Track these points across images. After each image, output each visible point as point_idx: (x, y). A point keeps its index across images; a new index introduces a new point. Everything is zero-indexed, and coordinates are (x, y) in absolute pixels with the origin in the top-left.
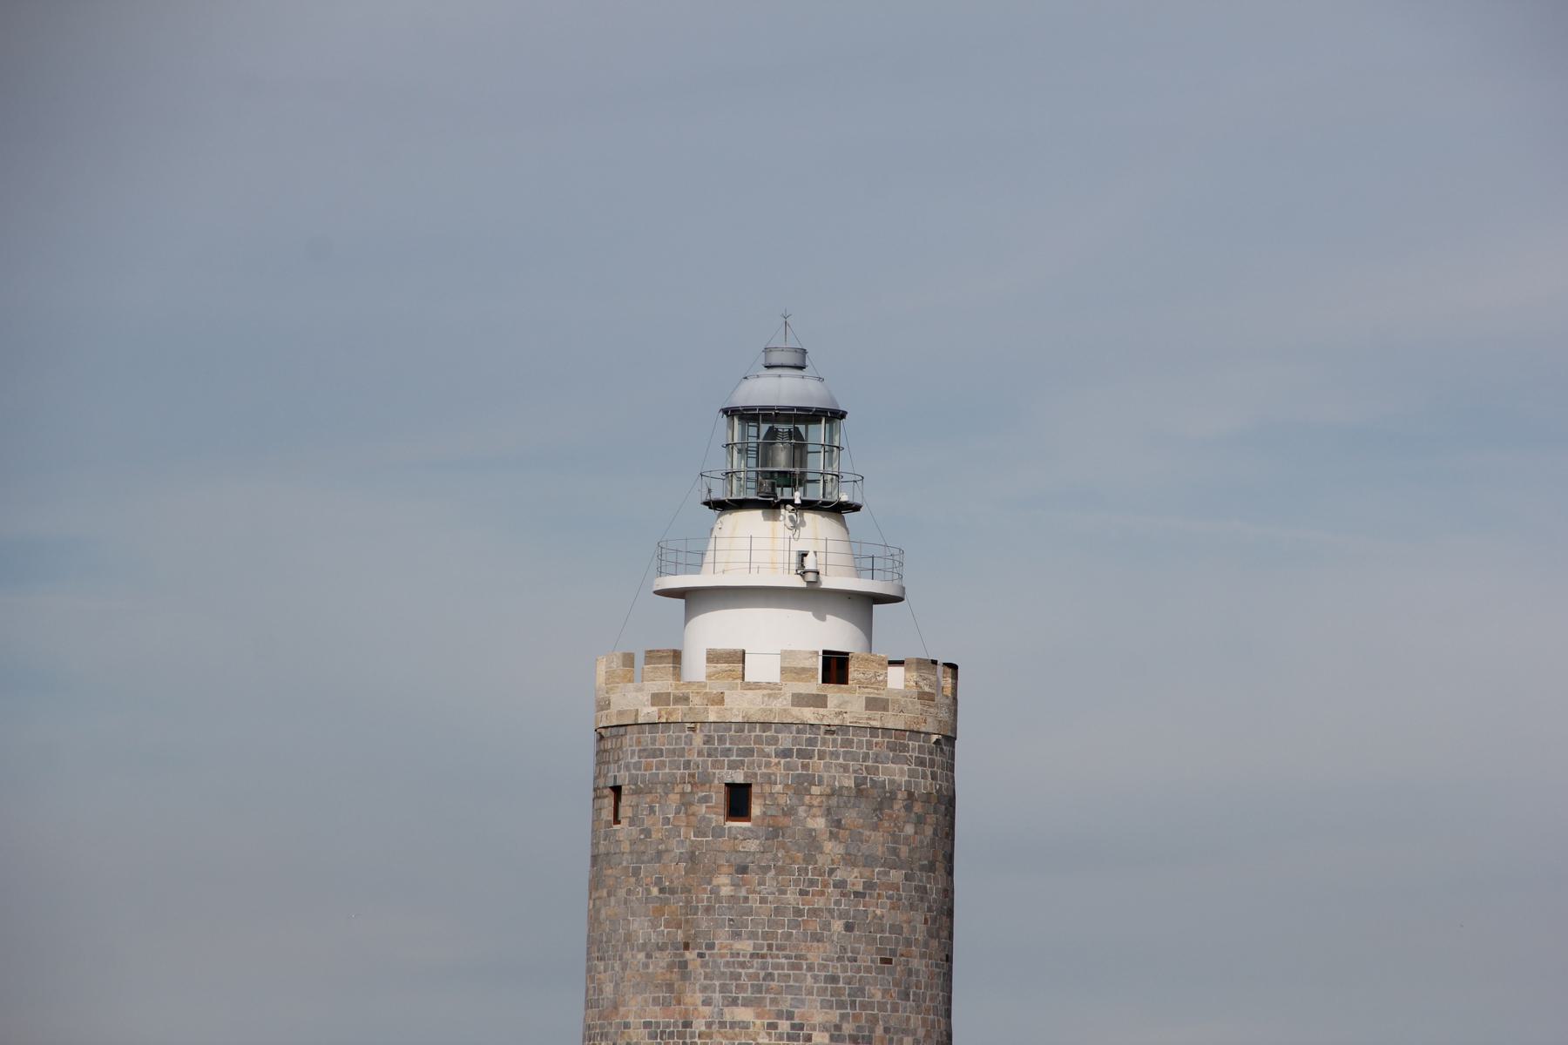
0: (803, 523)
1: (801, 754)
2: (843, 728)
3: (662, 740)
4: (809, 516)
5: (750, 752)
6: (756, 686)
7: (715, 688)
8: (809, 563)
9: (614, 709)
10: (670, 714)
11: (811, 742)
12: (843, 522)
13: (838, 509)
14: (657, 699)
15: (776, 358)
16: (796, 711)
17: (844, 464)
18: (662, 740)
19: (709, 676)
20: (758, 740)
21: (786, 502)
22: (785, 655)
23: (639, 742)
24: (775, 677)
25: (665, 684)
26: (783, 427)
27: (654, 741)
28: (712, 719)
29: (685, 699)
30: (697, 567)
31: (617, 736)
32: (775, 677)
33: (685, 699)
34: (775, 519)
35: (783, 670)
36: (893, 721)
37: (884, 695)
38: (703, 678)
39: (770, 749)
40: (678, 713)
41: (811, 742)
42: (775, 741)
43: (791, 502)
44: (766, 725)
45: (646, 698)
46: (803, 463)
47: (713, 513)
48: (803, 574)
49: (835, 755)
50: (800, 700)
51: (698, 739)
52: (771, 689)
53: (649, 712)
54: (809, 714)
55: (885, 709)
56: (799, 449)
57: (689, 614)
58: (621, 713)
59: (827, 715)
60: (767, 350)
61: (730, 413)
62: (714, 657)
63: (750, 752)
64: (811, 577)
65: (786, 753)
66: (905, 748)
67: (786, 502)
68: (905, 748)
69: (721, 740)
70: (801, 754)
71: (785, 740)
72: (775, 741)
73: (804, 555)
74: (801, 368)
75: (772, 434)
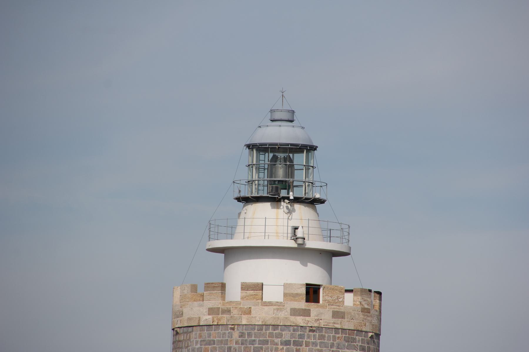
0: (294, 210)
1: (296, 343)
2: (320, 329)
3: (214, 335)
4: (297, 206)
5: (266, 342)
6: (270, 304)
7: (246, 305)
8: (299, 233)
9: (185, 317)
10: (219, 320)
11: (301, 336)
12: (315, 210)
13: (312, 202)
14: (212, 311)
15: (277, 116)
16: (292, 318)
17: (316, 176)
18: (214, 335)
19: (242, 298)
20: (271, 335)
21: (284, 198)
22: (286, 286)
23: (200, 336)
24: (280, 298)
25: (215, 302)
26: (281, 155)
27: (209, 335)
28: (244, 322)
29: (229, 311)
30: (231, 236)
31: (187, 333)
32: (280, 298)
33: (229, 311)
34: (278, 207)
35: (285, 295)
36: (348, 325)
37: (342, 309)
38: (239, 299)
39: (278, 341)
40: (224, 319)
41: (301, 336)
42: (280, 336)
43: (288, 198)
44: (275, 327)
45: (205, 310)
46: (292, 176)
47: (241, 204)
48: (296, 239)
49: (315, 344)
50: (295, 312)
51: (236, 335)
52: (279, 306)
53: (207, 319)
54: (300, 320)
55: (343, 317)
56: (290, 168)
57: (227, 263)
58: (190, 319)
59: (310, 321)
60: (272, 111)
61: (251, 147)
62: (245, 287)
63: (266, 342)
64: (300, 241)
65: (287, 343)
66: (354, 340)
67: (284, 198)
68: (354, 340)
69: (249, 335)
70: (296, 343)
71: (287, 335)
72: (280, 336)
73: (296, 228)
74: (292, 121)
75: (275, 159)
